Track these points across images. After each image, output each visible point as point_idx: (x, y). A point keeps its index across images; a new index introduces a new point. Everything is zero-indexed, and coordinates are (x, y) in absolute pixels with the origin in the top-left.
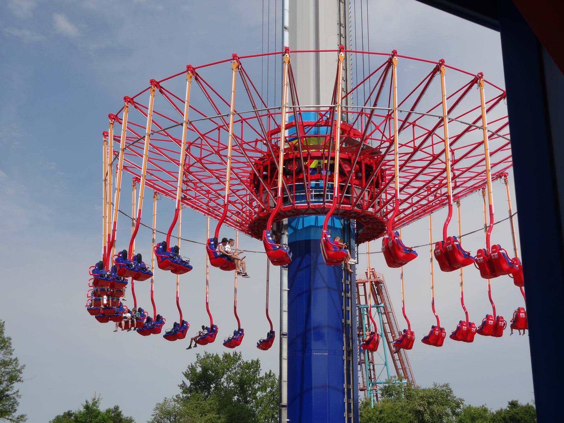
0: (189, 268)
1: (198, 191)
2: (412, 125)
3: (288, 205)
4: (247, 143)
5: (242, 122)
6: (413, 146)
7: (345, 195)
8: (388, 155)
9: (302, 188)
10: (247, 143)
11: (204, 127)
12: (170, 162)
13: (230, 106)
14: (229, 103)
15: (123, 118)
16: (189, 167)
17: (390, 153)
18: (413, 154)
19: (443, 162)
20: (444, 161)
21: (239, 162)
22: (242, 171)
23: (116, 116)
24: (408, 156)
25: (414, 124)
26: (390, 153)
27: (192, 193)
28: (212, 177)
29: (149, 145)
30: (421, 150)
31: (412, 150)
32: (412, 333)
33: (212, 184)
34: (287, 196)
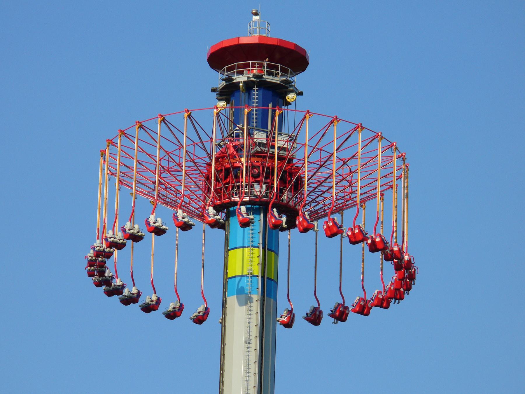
0: (291, 104)
1: (168, 192)
2: (320, 150)
3: (242, 177)
4: (171, 168)
5: (194, 145)
6: (319, 164)
7: (279, 66)
8: (313, 192)
9: (257, 155)
10: (171, 168)
11: (170, 147)
12: (173, 162)
13: (184, 134)
14: (183, 132)
15: (118, 142)
16: (161, 174)
17: (314, 192)
18: (319, 168)
19: (340, 175)
20: (341, 174)
21: (196, 174)
22: (199, 176)
23: (112, 140)
24: (324, 179)
25: (321, 150)
26: (314, 192)
27: (164, 192)
28: (197, 170)
29: (108, 166)
30: (324, 167)
31: (319, 166)
32: (321, 312)
33: (176, 185)
34: (234, 184)
